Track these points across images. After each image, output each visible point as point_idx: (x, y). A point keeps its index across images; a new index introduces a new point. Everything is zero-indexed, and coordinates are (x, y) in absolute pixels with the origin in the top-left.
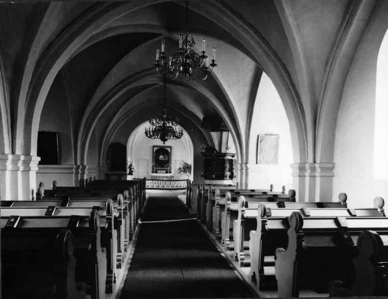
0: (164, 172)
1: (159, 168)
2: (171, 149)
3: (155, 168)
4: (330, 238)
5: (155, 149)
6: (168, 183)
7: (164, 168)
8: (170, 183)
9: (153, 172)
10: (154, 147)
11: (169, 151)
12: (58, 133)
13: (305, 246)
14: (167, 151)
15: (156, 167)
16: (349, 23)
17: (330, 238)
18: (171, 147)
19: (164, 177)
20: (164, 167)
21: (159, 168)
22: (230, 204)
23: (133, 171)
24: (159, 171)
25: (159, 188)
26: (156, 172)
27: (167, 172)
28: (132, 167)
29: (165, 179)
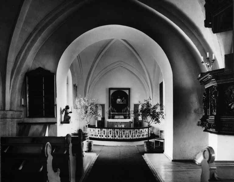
0: (122, 117)
1: (116, 113)
2: (129, 92)
3: (111, 113)
4: (215, 160)
5: (112, 92)
6: (127, 131)
7: (123, 113)
8: (130, 132)
9: (109, 118)
10: (110, 89)
11: (128, 93)
12: (27, 117)
13: (218, 178)
14: (125, 93)
15: (113, 111)
16: (140, 65)
17: (215, 160)
18: (129, 89)
19: (121, 123)
20: (122, 112)
21: (116, 113)
22: (90, 126)
23: (70, 118)
24: (116, 117)
25: (116, 138)
26: (113, 118)
27: (125, 118)
28: (69, 110)
29: (123, 126)
